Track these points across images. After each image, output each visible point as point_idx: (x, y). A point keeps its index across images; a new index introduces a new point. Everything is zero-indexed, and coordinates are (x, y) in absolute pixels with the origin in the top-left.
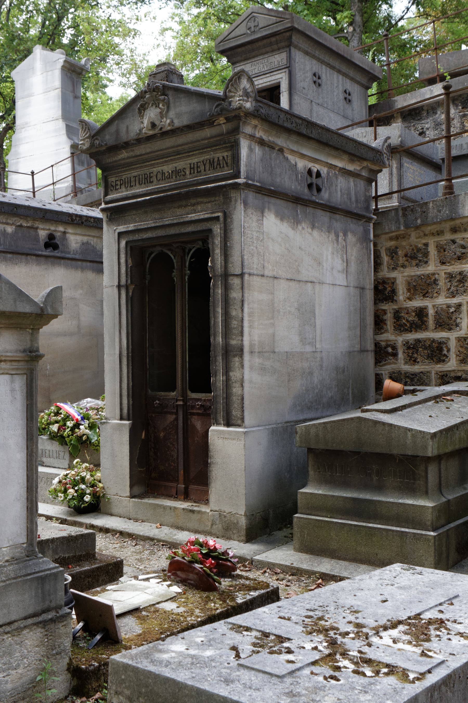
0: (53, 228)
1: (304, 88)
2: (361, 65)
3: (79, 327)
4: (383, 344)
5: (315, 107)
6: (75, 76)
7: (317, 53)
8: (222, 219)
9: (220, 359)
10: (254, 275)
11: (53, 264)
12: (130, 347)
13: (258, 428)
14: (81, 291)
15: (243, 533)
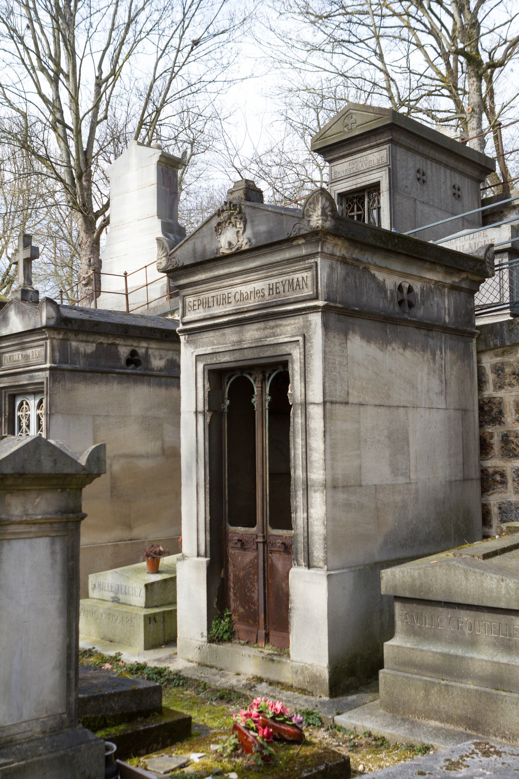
0: (135, 344)
1: (406, 187)
2: (470, 158)
3: (163, 449)
4: (491, 471)
5: (419, 206)
6: (170, 171)
7: (421, 148)
8: (301, 343)
9: (300, 493)
10: (336, 403)
11: (135, 382)
12: (208, 478)
13: (342, 571)
14: (166, 410)
15: (326, 687)
